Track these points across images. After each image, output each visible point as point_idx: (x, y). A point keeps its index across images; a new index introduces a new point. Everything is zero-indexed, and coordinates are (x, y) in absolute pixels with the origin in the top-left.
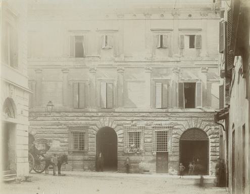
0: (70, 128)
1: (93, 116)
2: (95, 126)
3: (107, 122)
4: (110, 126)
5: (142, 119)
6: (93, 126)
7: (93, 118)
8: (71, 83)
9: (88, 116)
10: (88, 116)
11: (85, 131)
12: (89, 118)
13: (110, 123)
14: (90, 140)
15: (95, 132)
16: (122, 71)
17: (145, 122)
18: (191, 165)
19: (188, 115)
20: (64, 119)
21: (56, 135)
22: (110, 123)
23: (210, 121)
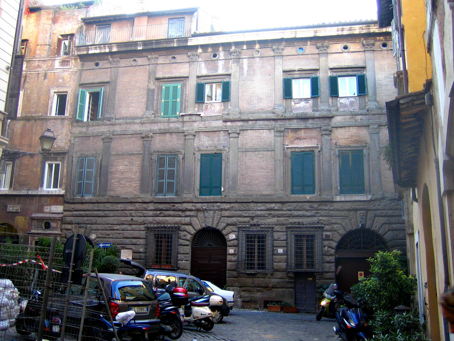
0: (148, 229)
1: (187, 210)
2: (190, 227)
3: (211, 220)
4: (214, 226)
5: (270, 214)
6: (186, 227)
7: (188, 213)
8: (155, 157)
9: (179, 210)
10: (179, 210)
11: (67, 114)
12: (180, 213)
13: (404, 106)
14: (182, 249)
15: (189, 237)
16: (236, 135)
17: (275, 220)
18: (335, 285)
19: (348, 206)
20: (141, 215)
21: (128, 241)
22: (404, 106)
23: (388, 216)
